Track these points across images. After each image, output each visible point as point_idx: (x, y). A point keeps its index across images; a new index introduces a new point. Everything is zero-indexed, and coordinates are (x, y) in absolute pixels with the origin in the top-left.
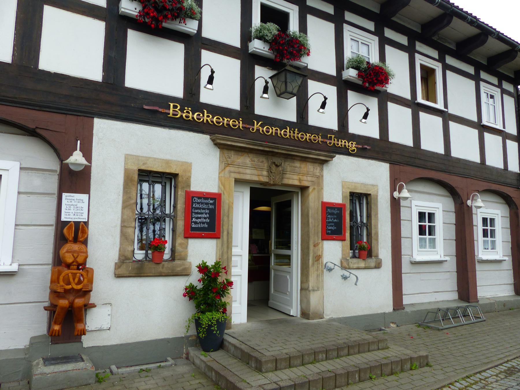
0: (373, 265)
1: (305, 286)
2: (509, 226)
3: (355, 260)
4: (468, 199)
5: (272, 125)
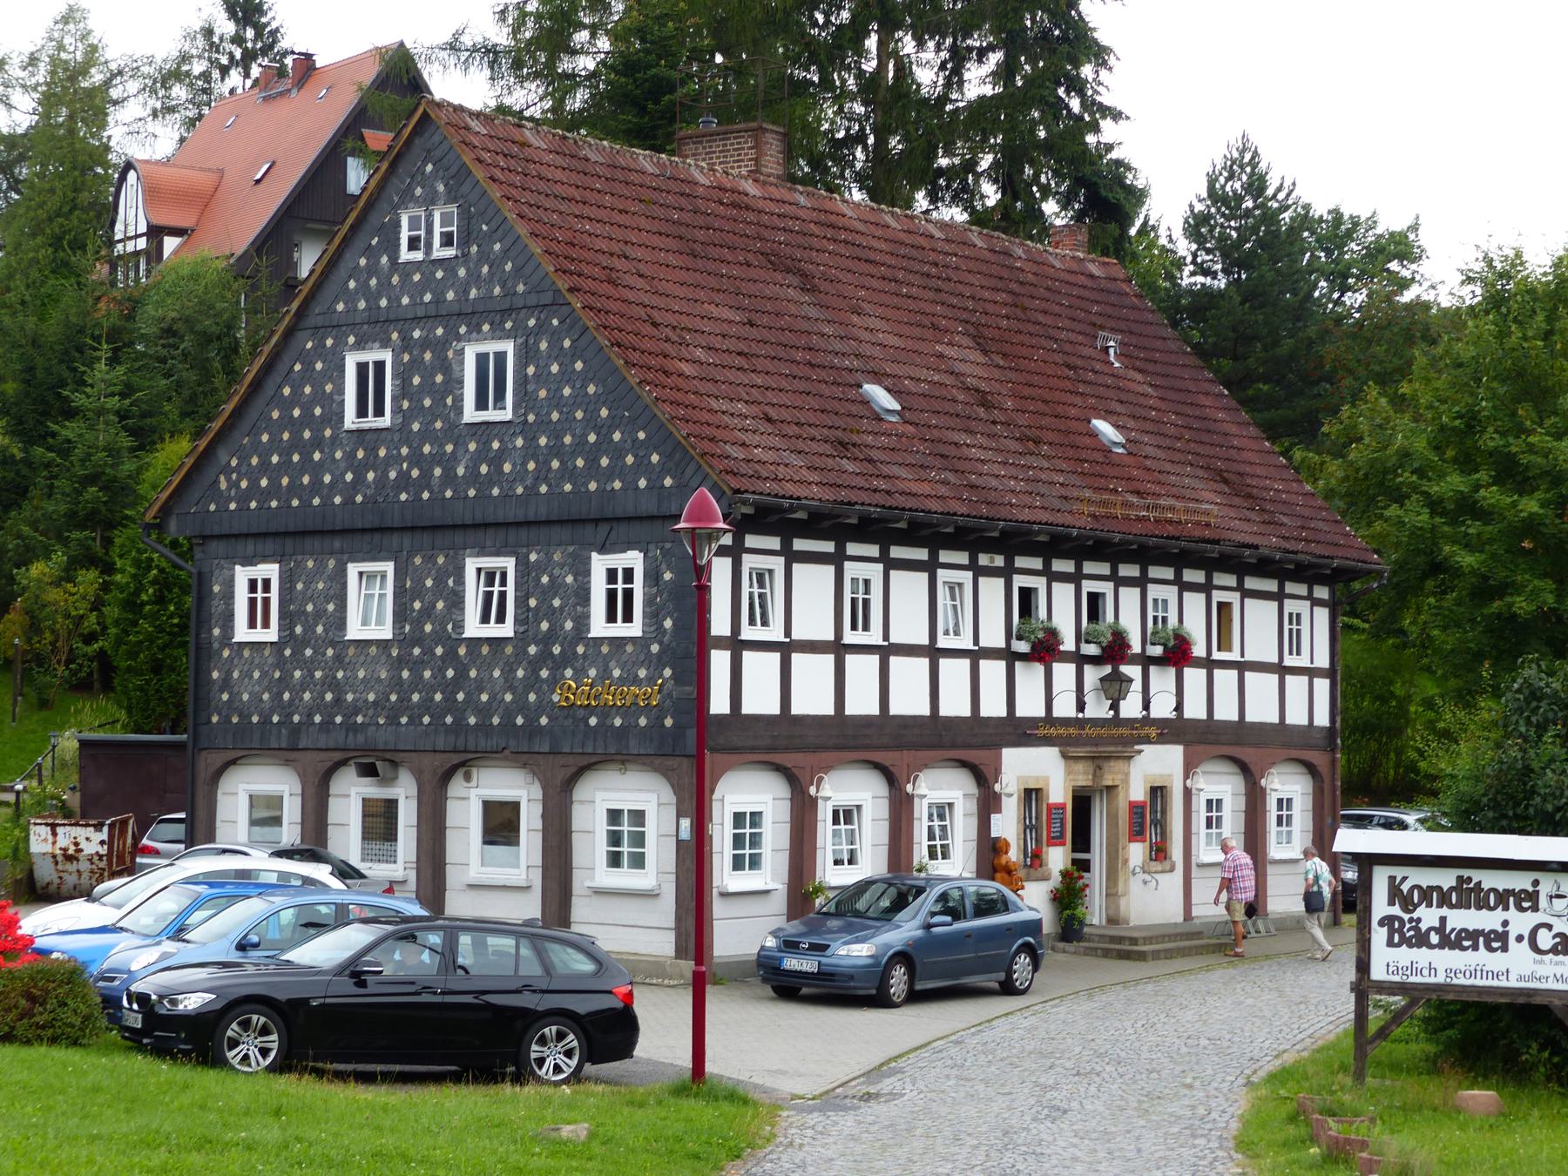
0: (1168, 868)
1: (1113, 891)
2: (1311, 808)
3: (1154, 863)
4: (908, 782)
5: (1096, 726)
